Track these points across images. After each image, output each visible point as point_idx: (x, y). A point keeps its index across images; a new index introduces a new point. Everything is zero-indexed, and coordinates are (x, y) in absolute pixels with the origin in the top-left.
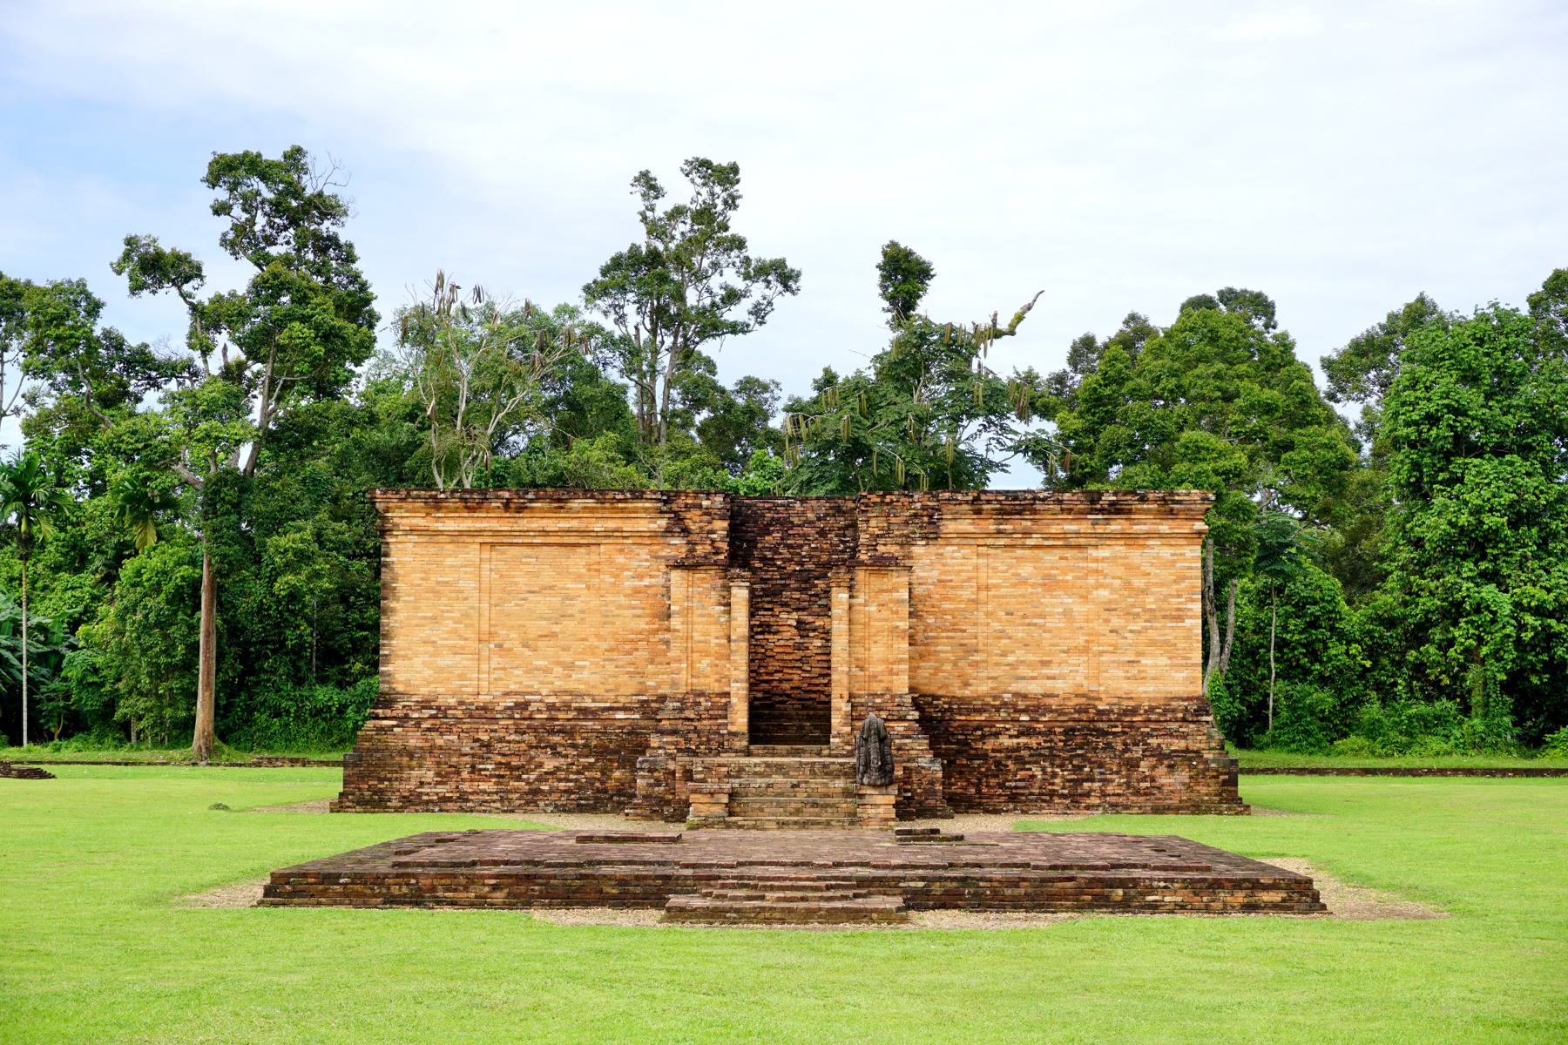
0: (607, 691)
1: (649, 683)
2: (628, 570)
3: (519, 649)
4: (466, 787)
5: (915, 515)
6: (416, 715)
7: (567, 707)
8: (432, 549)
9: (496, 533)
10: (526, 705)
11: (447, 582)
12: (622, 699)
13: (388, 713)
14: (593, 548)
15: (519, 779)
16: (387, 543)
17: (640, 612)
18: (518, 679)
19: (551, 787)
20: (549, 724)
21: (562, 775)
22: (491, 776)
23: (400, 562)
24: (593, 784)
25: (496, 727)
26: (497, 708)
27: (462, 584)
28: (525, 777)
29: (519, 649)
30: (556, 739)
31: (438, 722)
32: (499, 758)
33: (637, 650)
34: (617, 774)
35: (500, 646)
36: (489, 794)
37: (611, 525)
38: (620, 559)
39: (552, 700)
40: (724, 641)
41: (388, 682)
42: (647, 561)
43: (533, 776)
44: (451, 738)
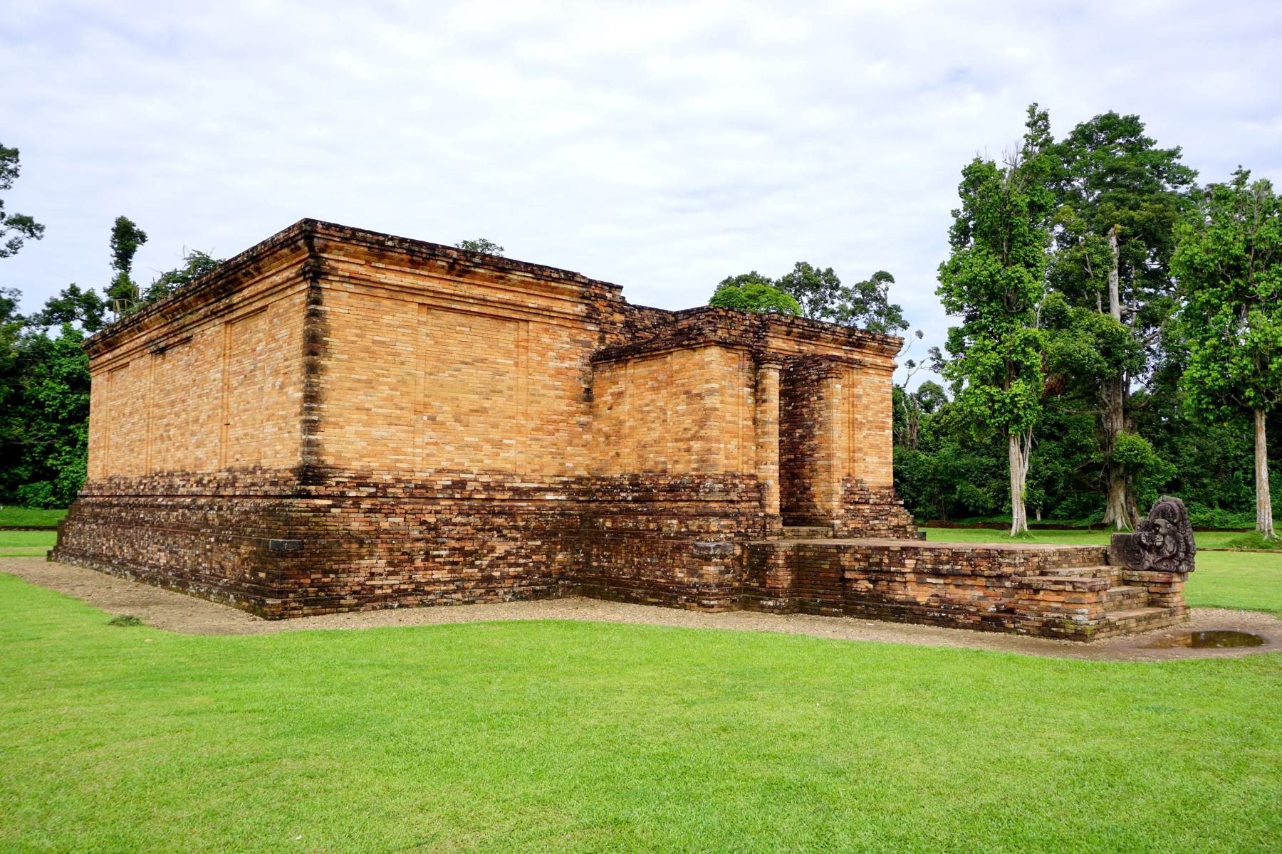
0: (533, 471)
1: (568, 465)
2: (552, 350)
3: (451, 423)
4: (419, 577)
5: (746, 331)
6: (353, 494)
7: (501, 487)
8: (369, 303)
9: (437, 294)
10: (461, 484)
11: (383, 343)
12: (547, 480)
13: (322, 490)
14: (522, 324)
15: (472, 565)
16: (320, 289)
17: (561, 393)
18: (450, 456)
19: (502, 573)
20: (487, 504)
21: (512, 559)
22: (445, 563)
23: (334, 313)
24: (539, 568)
25: (438, 508)
26: (436, 487)
27: (399, 346)
28: (478, 563)
29: (451, 423)
30: (500, 521)
31: (377, 501)
32: (453, 543)
33: (558, 430)
34: (560, 557)
35: (432, 419)
36: (445, 583)
37: (544, 303)
38: (546, 339)
39: (485, 479)
40: (750, 423)
41: (317, 454)
42: (567, 343)
43: (485, 562)
44: (397, 520)
